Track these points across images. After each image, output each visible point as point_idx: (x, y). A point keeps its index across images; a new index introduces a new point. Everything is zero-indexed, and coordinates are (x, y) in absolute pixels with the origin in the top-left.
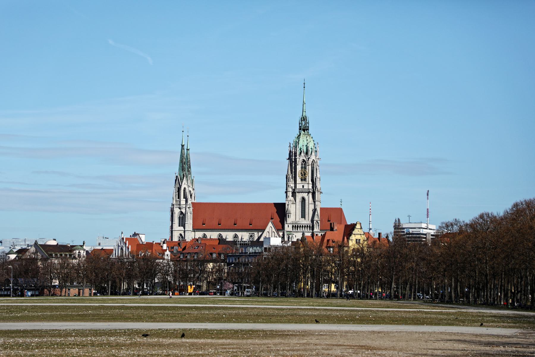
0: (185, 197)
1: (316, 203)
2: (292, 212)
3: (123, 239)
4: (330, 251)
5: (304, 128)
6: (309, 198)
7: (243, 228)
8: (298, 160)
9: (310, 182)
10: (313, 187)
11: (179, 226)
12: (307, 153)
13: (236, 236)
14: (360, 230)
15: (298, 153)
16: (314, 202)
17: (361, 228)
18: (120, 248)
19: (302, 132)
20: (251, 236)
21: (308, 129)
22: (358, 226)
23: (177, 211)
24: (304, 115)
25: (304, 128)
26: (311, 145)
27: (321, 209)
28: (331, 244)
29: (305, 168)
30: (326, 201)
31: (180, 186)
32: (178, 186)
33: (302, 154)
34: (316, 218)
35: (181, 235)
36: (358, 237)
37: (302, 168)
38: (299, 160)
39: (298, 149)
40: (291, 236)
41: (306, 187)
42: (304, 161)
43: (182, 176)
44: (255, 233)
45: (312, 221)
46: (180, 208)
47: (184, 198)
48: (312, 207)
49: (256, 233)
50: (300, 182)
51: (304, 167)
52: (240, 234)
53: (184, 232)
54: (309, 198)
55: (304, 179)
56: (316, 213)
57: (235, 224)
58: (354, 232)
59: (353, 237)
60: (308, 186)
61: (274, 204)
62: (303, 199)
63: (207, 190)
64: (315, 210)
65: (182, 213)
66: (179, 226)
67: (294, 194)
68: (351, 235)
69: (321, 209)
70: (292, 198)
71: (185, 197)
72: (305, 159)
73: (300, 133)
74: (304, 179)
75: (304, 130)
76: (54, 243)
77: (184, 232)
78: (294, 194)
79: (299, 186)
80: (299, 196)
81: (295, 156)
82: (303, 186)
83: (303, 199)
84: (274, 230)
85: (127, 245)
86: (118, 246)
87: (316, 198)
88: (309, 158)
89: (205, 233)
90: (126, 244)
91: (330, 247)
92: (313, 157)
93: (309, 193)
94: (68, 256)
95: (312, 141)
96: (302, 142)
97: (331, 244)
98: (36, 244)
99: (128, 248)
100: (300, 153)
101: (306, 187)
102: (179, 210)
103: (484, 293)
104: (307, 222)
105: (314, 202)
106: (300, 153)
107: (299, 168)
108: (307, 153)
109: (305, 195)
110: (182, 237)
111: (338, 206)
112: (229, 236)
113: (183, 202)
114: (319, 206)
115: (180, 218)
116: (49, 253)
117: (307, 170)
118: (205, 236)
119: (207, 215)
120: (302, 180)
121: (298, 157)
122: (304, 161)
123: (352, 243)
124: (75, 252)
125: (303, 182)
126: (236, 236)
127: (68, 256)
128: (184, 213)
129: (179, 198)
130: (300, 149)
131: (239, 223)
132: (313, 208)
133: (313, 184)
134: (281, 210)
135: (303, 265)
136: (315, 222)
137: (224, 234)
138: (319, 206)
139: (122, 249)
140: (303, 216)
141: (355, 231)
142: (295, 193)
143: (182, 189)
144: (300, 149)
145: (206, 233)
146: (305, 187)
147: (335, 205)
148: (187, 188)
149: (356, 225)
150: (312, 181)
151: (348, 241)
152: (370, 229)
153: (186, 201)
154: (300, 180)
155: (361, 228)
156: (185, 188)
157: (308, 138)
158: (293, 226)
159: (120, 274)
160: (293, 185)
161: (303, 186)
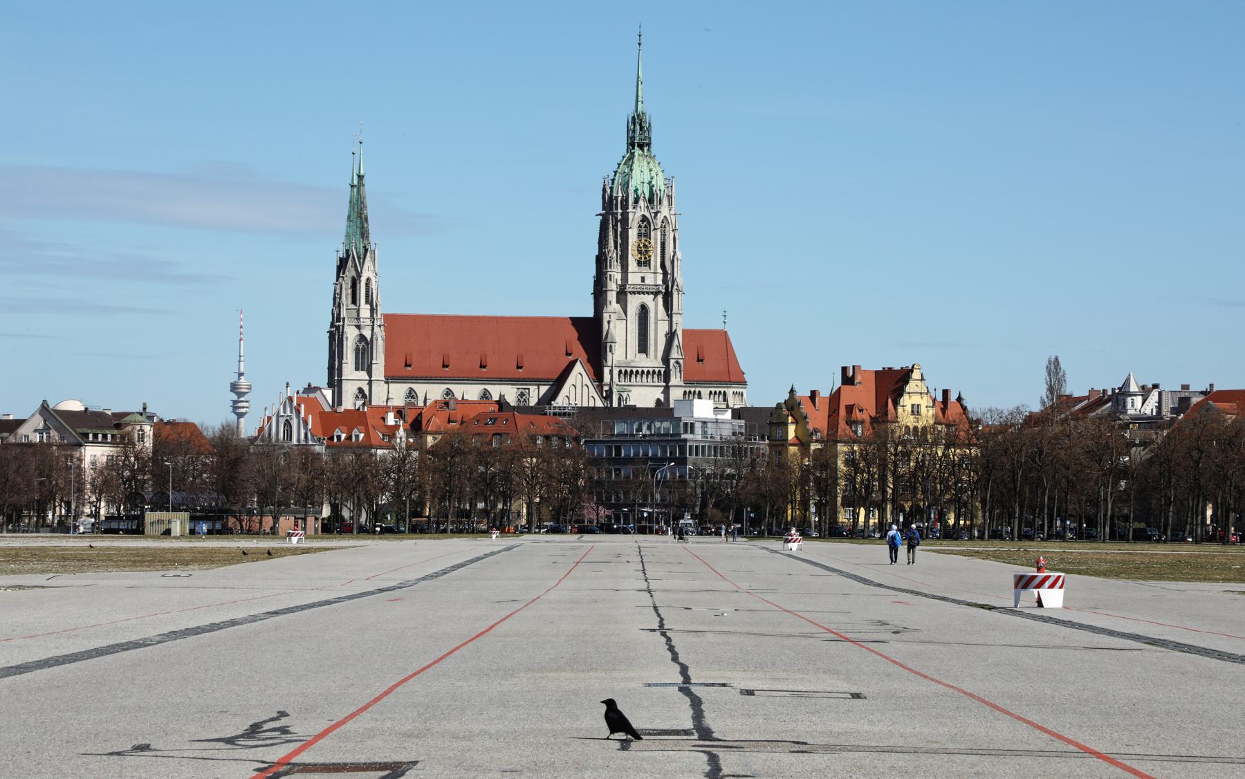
0: (369, 300)
1: (675, 318)
2: (617, 339)
3: (290, 399)
4: (855, 433)
5: (639, 137)
6: (656, 305)
7: (503, 376)
8: (631, 216)
9: (660, 271)
10: (665, 281)
11: (357, 369)
12: (651, 201)
13: (411, 394)
14: (919, 383)
15: (631, 200)
16: (670, 316)
17: (922, 379)
18: (282, 421)
19: (637, 151)
20: (522, 395)
21: (649, 145)
22: (916, 375)
23: (351, 334)
24: (640, 110)
25: (639, 137)
26: (659, 183)
27: (685, 332)
28: (857, 415)
29: (648, 236)
30: (693, 314)
31: (359, 275)
32: (354, 274)
33: (641, 203)
34: (675, 354)
35: (361, 390)
36: (916, 400)
37: (640, 235)
38: (634, 216)
39: (631, 190)
40: (625, 395)
41: (650, 280)
42: (644, 219)
43: (362, 251)
44: (532, 388)
45: (666, 359)
46: (358, 327)
47: (367, 302)
48: (664, 328)
49: (533, 389)
50: (636, 269)
51: (645, 233)
52: (421, 389)
53: (370, 383)
54: (656, 307)
55: (644, 263)
56: (676, 343)
57: (482, 366)
58: (908, 389)
59: (907, 401)
60: (655, 279)
61: (572, 319)
62: (644, 310)
63: (408, 284)
64: (671, 336)
65: (362, 338)
66: (357, 369)
67: (622, 295)
68: (901, 395)
69: (685, 332)
70: (617, 307)
71: (369, 300)
72: (648, 215)
73: (633, 154)
74: (644, 263)
75: (641, 146)
76: (75, 406)
77: (370, 383)
78: (622, 295)
79: (634, 279)
80: (634, 302)
81: (625, 206)
82: (643, 279)
83: (644, 310)
84: (587, 381)
85: (302, 415)
86: (278, 416)
87: (675, 307)
88: (656, 214)
89: (413, 386)
90: (298, 412)
91: (856, 422)
92: (664, 211)
93: (656, 294)
94: (91, 436)
95: (660, 173)
96: (640, 176)
97: (857, 415)
98: (45, 409)
99: (306, 423)
100: (636, 201)
101: (650, 280)
102: (357, 332)
103: (54, 513)
104: (653, 361)
105: (670, 316)
106: (636, 201)
107: (633, 234)
108: (651, 201)
109: (648, 300)
110: (364, 396)
111: (716, 325)
112: (510, 393)
113: (365, 312)
114: (680, 324)
115: (357, 350)
116: (80, 430)
117: (652, 241)
118: (449, 392)
119: (422, 345)
120: (639, 263)
121: (630, 209)
122: (644, 219)
123: (905, 417)
124: (129, 428)
125: (643, 269)
126: (411, 394)
127: (91, 436)
128: (369, 337)
129: (354, 302)
130: (636, 191)
131: (491, 363)
132: (666, 329)
133: (665, 274)
134: (591, 335)
135: (186, 454)
136: (672, 362)
137: (459, 390)
138: (680, 324)
139: (288, 424)
140: (643, 348)
141: (911, 386)
142: (625, 293)
143: (363, 280)
144: (636, 191)
145: (452, 387)
146: (647, 282)
147: (714, 324)
148: (373, 280)
149: (912, 371)
150: (663, 266)
151: (895, 409)
152: (241, 374)
153: (373, 310)
154: (635, 264)
155: (922, 379)
156: (368, 279)
157: (651, 165)
158: (620, 372)
159: (211, 486)
160: (618, 276)
161: (643, 279)
